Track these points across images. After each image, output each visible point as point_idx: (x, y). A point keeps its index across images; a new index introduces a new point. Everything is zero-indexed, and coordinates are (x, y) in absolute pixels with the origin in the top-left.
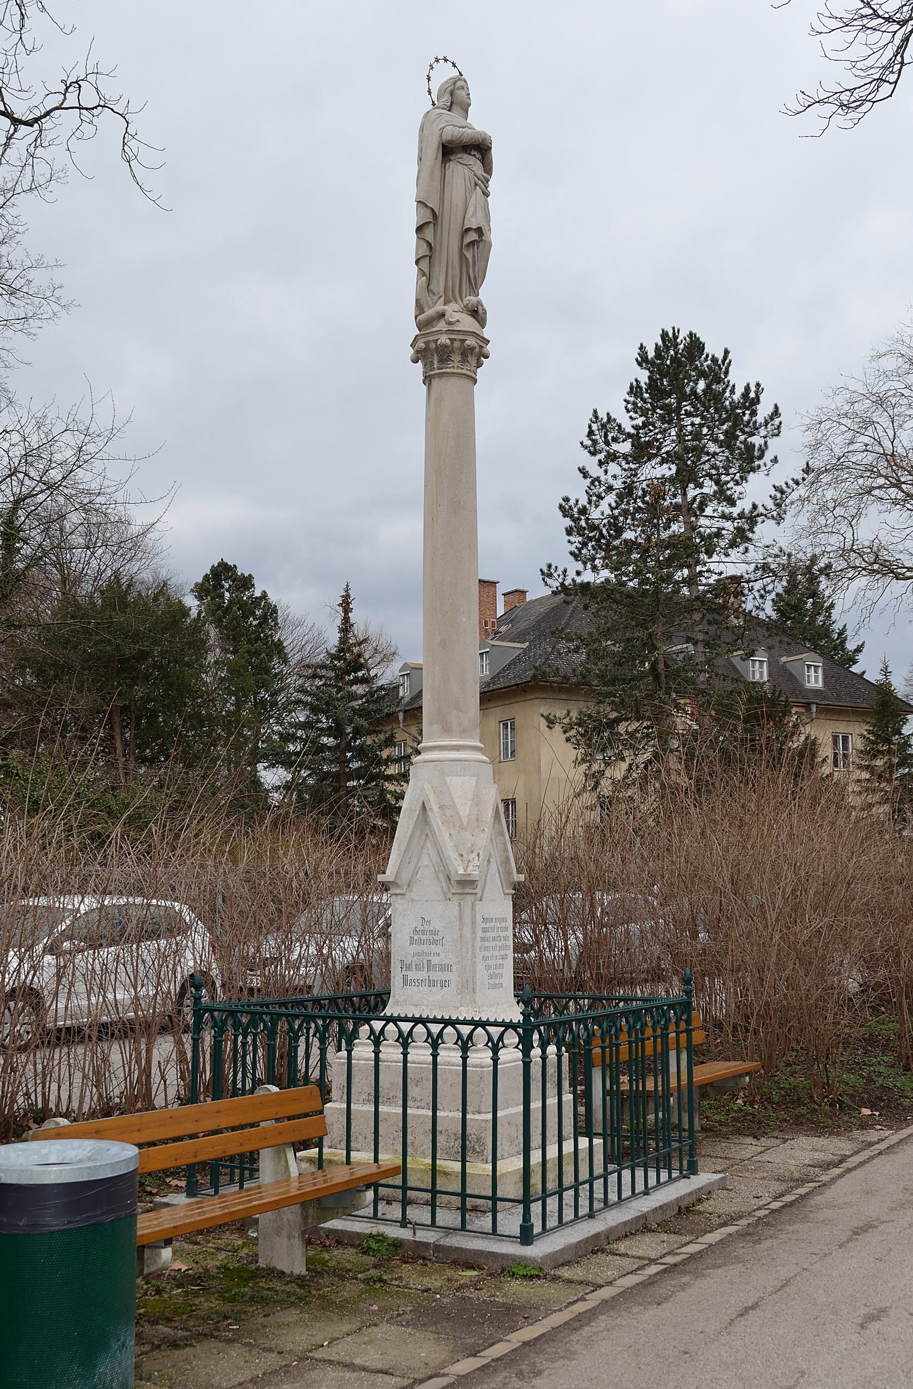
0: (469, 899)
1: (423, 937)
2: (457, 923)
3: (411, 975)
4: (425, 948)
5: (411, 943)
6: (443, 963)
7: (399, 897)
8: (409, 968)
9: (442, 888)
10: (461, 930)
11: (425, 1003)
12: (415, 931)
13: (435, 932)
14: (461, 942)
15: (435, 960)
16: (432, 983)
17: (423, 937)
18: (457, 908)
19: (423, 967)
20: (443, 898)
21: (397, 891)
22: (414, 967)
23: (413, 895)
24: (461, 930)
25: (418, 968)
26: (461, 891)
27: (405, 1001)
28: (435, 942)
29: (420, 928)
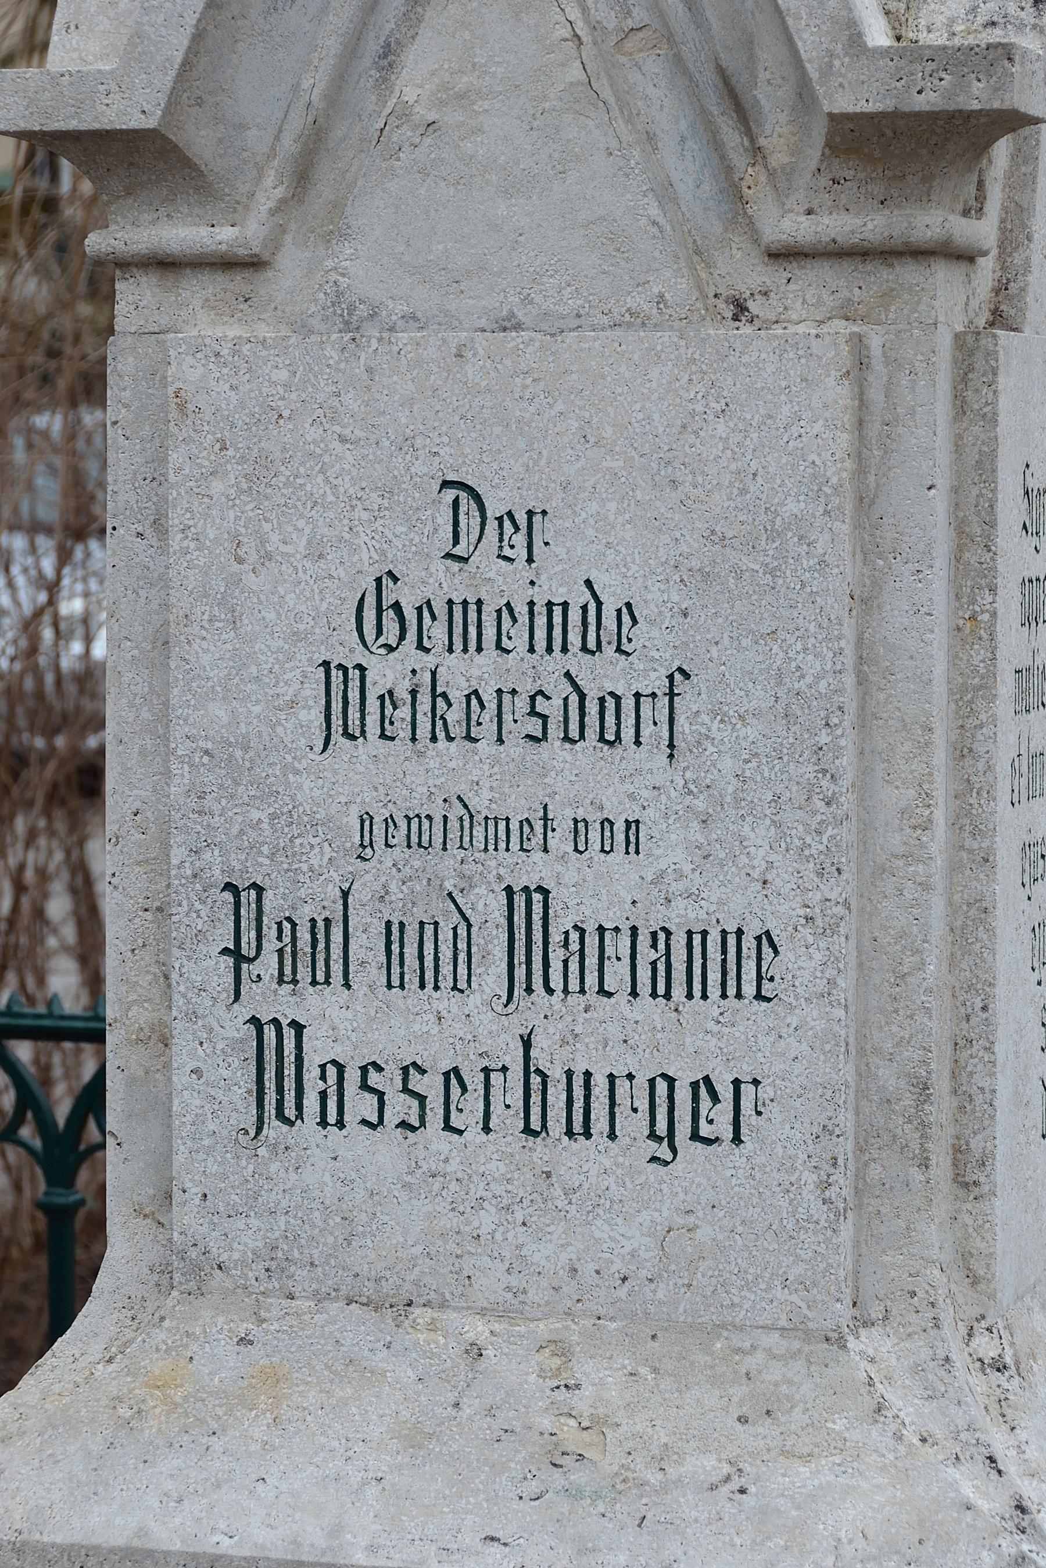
0: (951, 299)
1: (461, 672)
2: (835, 539)
3: (339, 1024)
4: (490, 775)
5: (339, 725)
6: (680, 916)
7: (198, 289)
8: (315, 952)
9: (665, 193)
10: (865, 601)
11: (492, 1282)
12: (381, 612)
13: (594, 624)
14: (865, 720)
15: (590, 892)
16: (561, 1106)
17: (461, 672)
18: (837, 393)
19: (466, 954)
20: (678, 287)
21: (182, 233)
22: (367, 946)
23: (361, 266)
24: (865, 601)
25: (416, 957)
26: (870, 225)
27: (275, 1263)
28: (598, 721)
29: (425, 581)
